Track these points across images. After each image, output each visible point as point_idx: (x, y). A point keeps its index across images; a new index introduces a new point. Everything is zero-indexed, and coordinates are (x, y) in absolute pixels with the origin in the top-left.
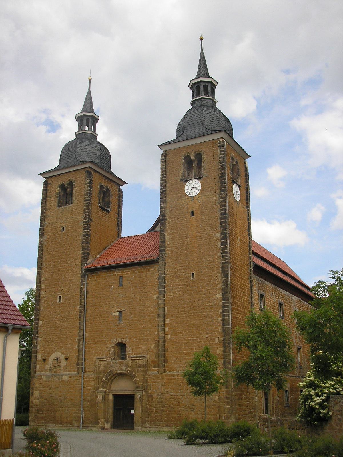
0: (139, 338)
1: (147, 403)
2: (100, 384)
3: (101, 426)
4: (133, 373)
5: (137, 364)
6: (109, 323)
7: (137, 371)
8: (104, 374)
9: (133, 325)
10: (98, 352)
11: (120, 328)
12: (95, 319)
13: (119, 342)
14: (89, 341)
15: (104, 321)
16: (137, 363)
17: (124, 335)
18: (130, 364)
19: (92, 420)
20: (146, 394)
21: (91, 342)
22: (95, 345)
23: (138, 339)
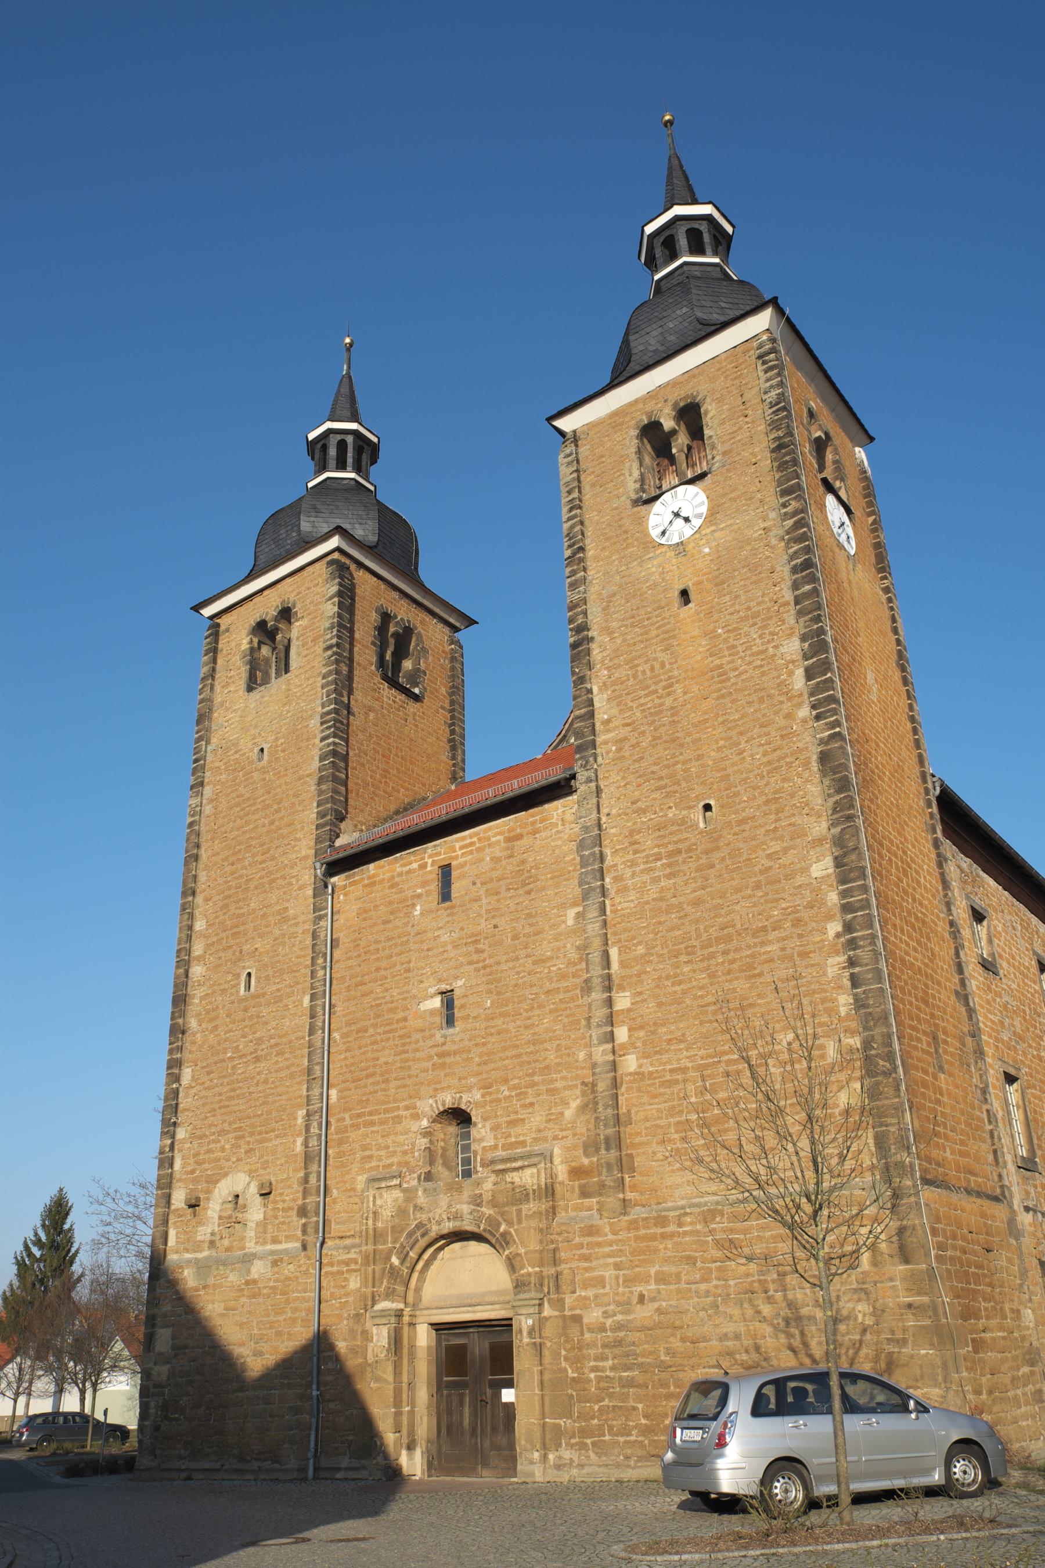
0: (516, 1081)
1: (563, 1353)
2: (382, 1283)
4: (499, 1225)
5: (513, 1189)
6: (408, 1040)
9: (492, 1034)
11: (448, 1054)
14: (340, 1116)
15: (391, 1035)
16: (513, 1183)
18: (487, 1191)
19: (351, 1438)
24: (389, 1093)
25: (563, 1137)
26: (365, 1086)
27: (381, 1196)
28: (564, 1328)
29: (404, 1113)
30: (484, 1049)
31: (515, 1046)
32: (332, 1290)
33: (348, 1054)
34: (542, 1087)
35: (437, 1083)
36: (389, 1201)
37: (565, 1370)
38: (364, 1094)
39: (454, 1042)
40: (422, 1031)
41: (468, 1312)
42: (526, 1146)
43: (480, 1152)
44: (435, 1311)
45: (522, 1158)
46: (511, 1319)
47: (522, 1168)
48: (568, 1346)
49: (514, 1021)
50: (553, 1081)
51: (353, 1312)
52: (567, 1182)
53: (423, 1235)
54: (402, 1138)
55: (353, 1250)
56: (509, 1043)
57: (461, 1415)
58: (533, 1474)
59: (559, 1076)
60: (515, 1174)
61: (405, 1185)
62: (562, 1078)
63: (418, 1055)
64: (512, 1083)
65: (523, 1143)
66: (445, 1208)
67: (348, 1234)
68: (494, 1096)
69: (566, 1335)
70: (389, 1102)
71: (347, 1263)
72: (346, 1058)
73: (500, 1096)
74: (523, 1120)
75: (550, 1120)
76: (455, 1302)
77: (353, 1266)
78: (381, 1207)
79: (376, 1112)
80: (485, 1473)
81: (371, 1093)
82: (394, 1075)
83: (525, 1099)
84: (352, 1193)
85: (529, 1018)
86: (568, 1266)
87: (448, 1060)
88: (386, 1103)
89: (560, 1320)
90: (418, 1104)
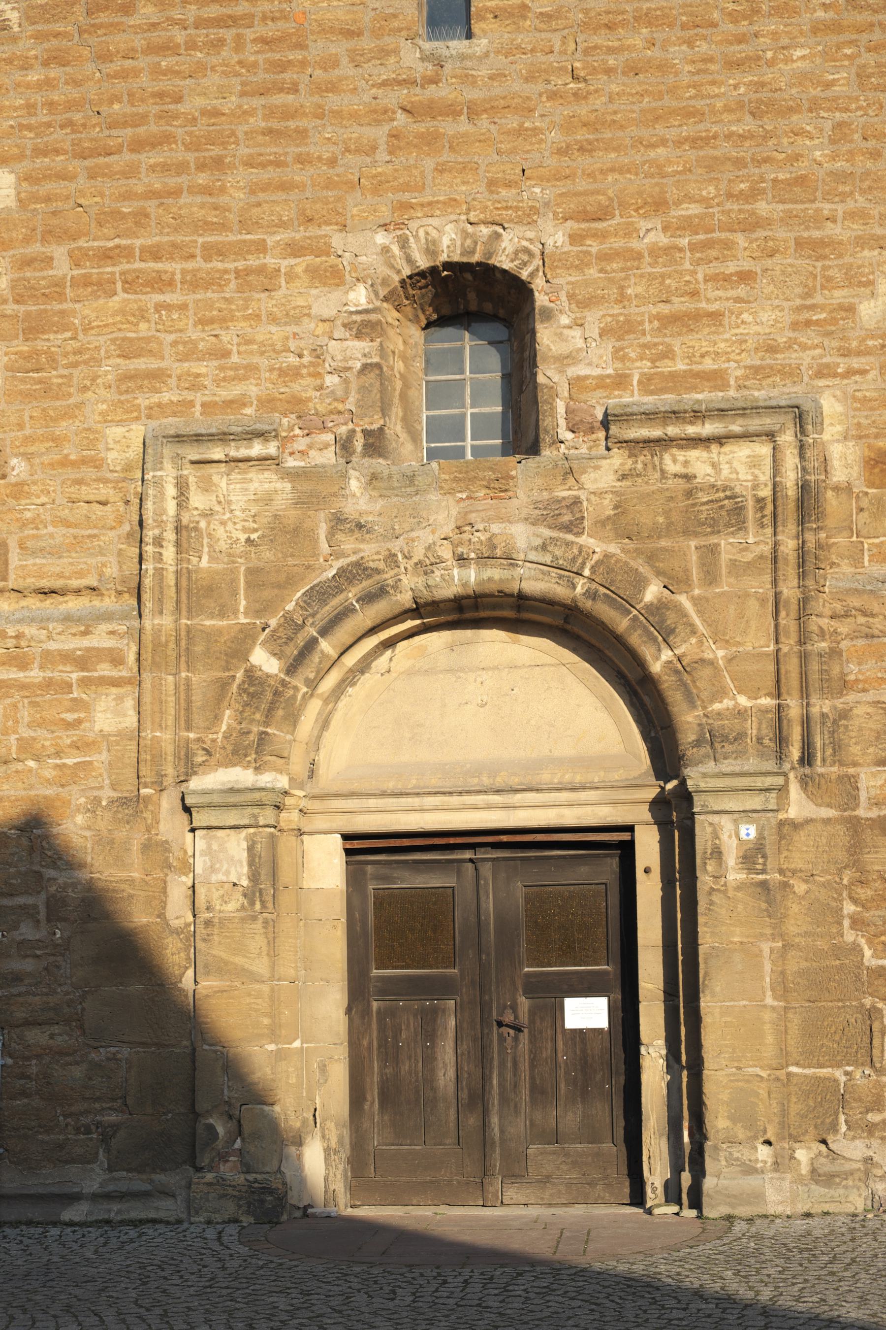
0: (694, 209)
1: (849, 908)
2: (217, 718)
3: (241, 1179)
4: (640, 584)
5: (689, 494)
6: (295, 55)
7: (702, 565)
8: (261, 609)
9: (609, 71)
10: (157, 377)
11: (451, 111)
12: (103, 18)
13: (444, 257)
14: (36, 248)
15: (229, 34)
16: (688, 477)
17: (509, 185)
18: (600, 494)
19: (113, 1118)
20: (831, 813)
21: (62, 267)
22: (115, 302)
23: (688, 225)
24: (224, 200)
25: (850, 373)
26: (131, 172)
27: (207, 486)
28: (856, 848)
29: (285, 264)
30: (583, 110)
31: (690, 114)
32: (26, 733)
33: (54, 72)
34: (781, 233)
35: (406, 187)
36: (239, 501)
37: (856, 949)
38: (127, 196)
39: (468, 79)
40: (350, 34)
41: (489, 807)
42: (725, 387)
43: (564, 390)
44: (373, 803)
45: (721, 413)
46: (630, 829)
47: (720, 440)
48: (863, 893)
49: (690, 43)
50: (819, 220)
51: (107, 794)
52: (859, 487)
53: (368, 598)
54: (276, 332)
55: (104, 627)
56: (668, 102)
57: (430, 1059)
58: (759, 1197)
59: (840, 208)
60: (694, 454)
61: (291, 463)
62: (851, 215)
63: (333, 101)
64: (676, 213)
65: (717, 379)
66: (448, 529)
67: (75, 583)
68: (618, 243)
69: (857, 864)
70: (224, 227)
71: (83, 661)
72: (48, 84)
73: (635, 244)
74: (715, 317)
75: (808, 323)
76: (434, 782)
77: (105, 670)
78: (208, 514)
79: (176, 251)
80: (511, 1194)
81: (151, 194)
82: (244, 151)
83: (724, 259)
84: (89, 472)
85: (741, 39)
86: (870, 696)
87: (448, 127)
88: (208, 227)
89: (841, 829)
90: (337, 241)
